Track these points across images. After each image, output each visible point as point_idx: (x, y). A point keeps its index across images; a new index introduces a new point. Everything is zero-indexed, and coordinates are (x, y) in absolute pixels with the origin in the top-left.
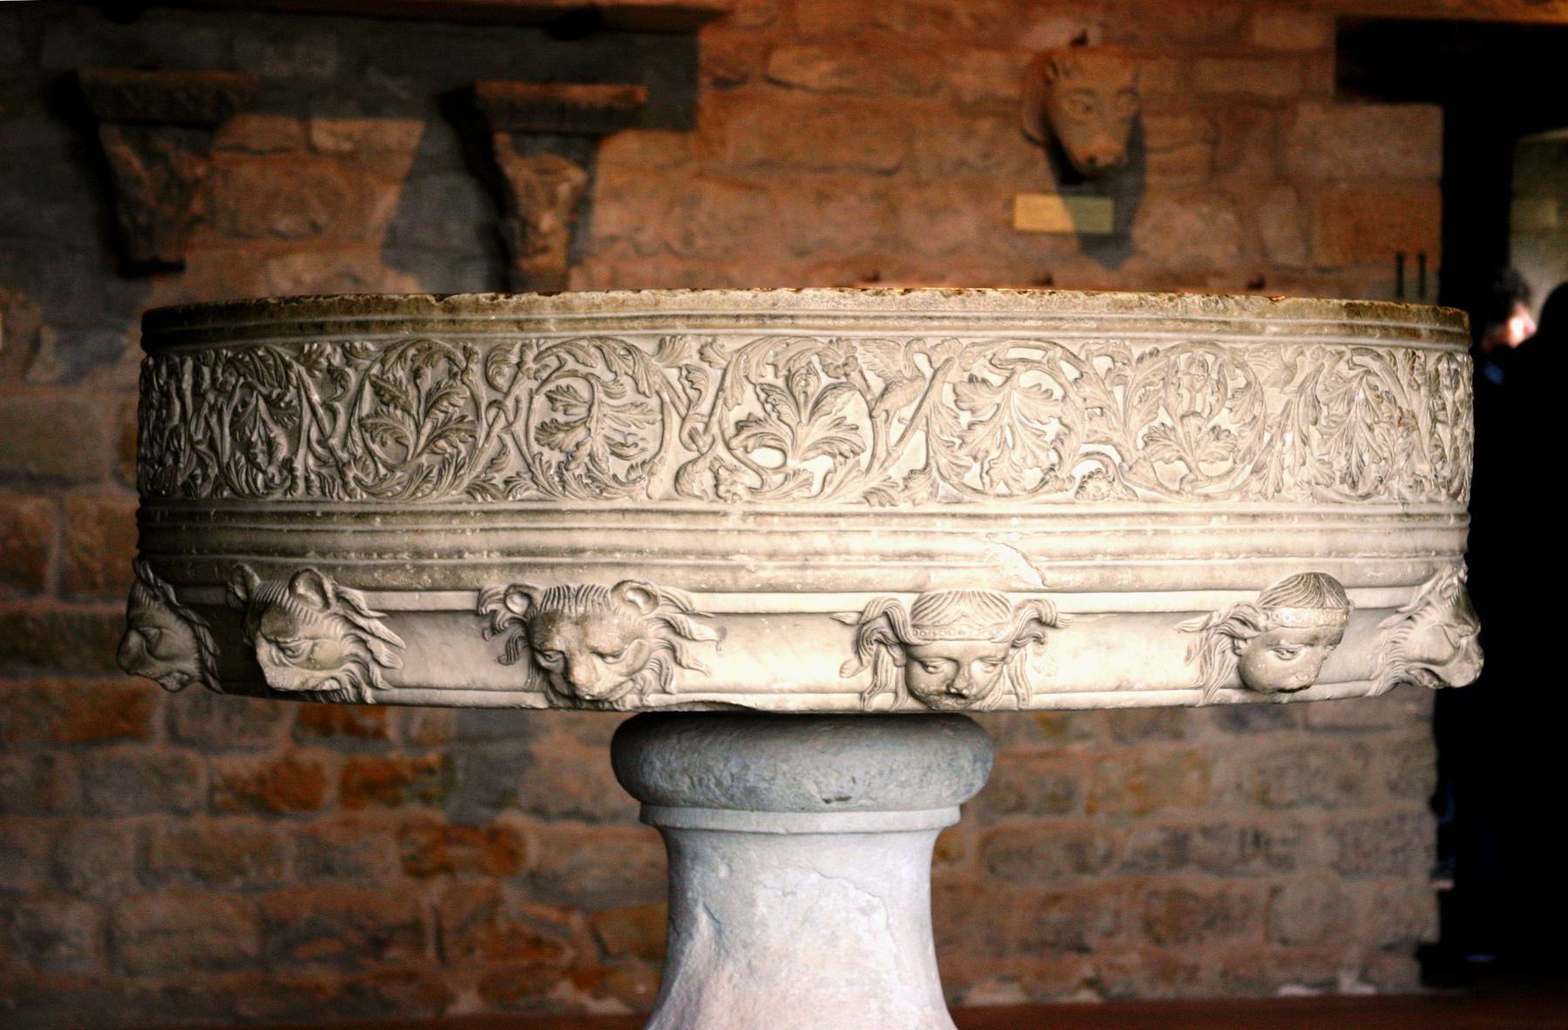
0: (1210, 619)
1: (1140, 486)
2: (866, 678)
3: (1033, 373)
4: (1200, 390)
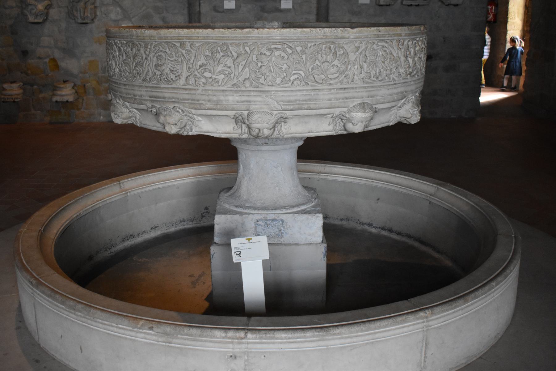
2: (239, 131)
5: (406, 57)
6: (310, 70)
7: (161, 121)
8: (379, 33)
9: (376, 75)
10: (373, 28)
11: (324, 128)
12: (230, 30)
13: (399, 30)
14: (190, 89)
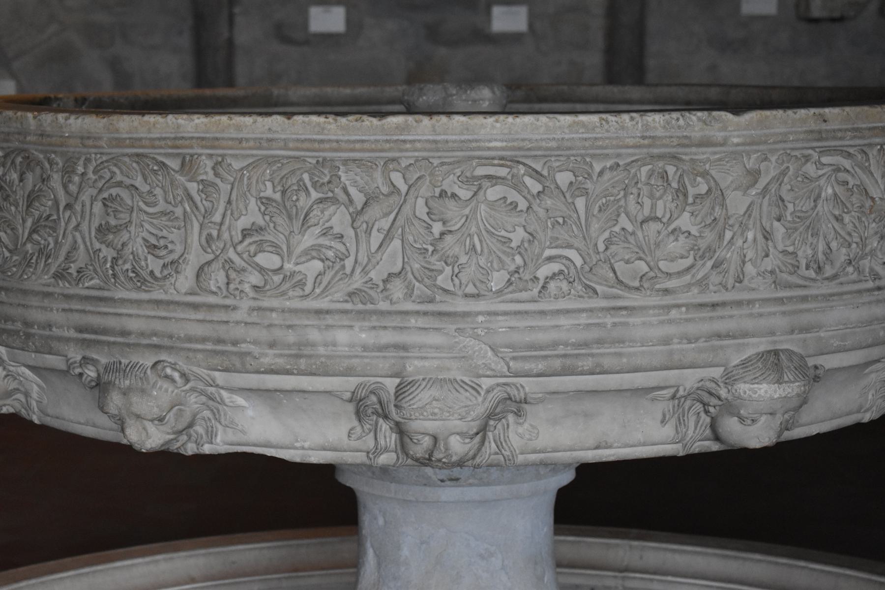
0: (677, 391)
1: (601, 284)
3: (498, 188)
4: (660, 198)
6: (601, 247)
7: (113, 410)
8: (824, 127)
9: (816, 261)
10: (802, 112)
11: (645, 434)
12: (343, 120)
14: (211, 307)
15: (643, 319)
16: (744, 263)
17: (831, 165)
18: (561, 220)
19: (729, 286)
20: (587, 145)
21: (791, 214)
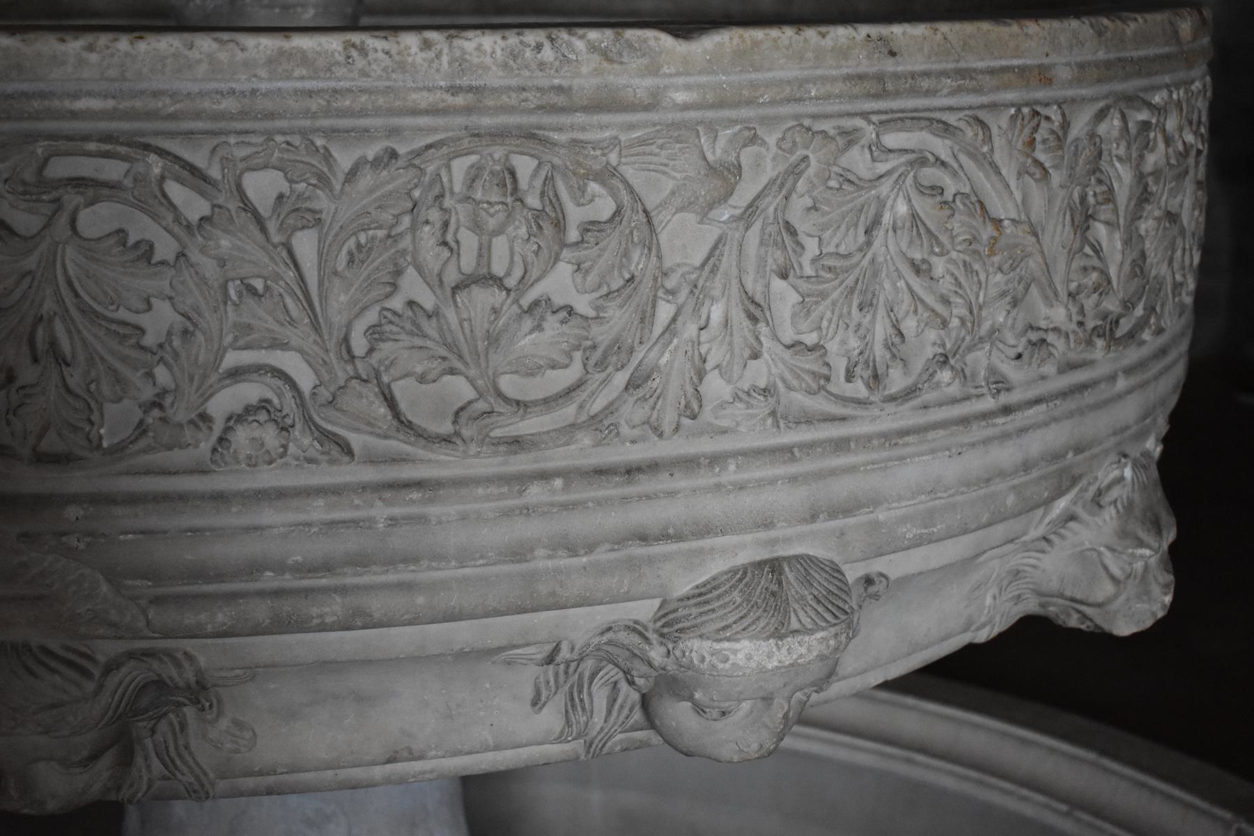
1: (357, 430)
4: (499, 231)
5: (1083, 219)
8: (889, 66)
9: (871, 365)
10: (840, 33)
13: (1032, 40)
15: (461, 507)
16: (701, 374)
17: (906, 151)
18: (259, 284)
19: (667, 428)
20: (314, 108)
21: (814, 261)
